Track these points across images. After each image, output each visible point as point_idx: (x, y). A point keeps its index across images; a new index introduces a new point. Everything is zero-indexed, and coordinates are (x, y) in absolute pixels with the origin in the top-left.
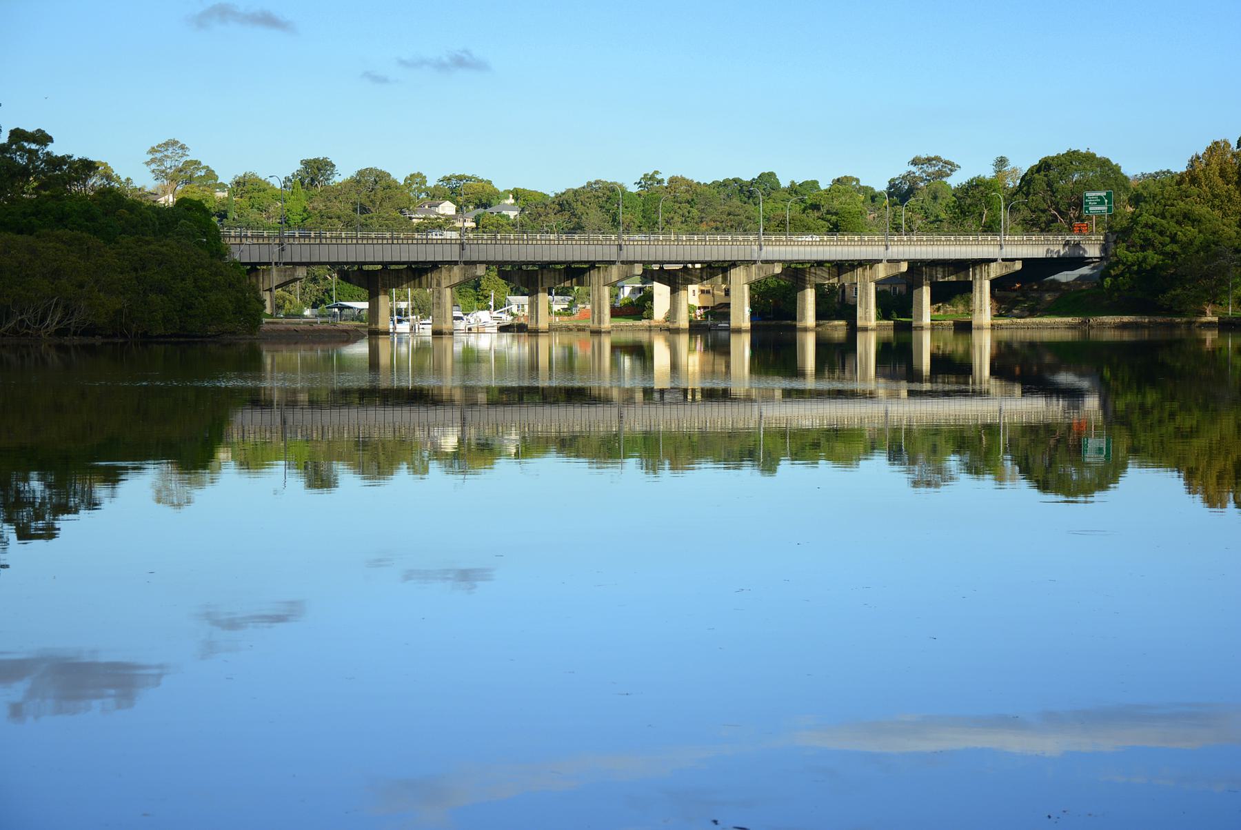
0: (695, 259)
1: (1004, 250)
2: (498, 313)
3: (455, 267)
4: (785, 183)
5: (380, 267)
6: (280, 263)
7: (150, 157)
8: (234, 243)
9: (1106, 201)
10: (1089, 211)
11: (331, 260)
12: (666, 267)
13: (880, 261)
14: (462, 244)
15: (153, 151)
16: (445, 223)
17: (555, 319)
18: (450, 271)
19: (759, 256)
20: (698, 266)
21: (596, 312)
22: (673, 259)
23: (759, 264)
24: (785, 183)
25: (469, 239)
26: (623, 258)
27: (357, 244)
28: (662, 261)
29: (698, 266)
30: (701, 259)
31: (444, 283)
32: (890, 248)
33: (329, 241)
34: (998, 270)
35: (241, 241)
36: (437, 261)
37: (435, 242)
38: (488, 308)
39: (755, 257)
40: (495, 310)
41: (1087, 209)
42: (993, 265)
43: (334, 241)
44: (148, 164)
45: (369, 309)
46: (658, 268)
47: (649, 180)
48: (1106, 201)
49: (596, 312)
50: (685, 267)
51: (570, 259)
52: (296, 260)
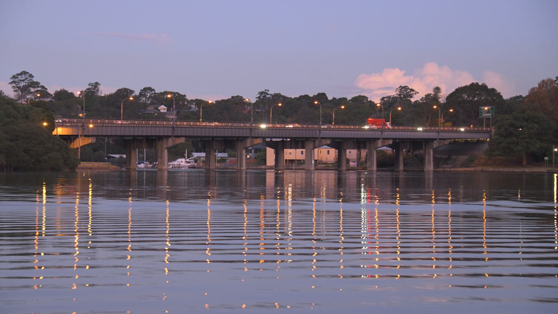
0: (287, 136)
1: (440, 134)
2: (189, 160)
3: (317, 140)
4: (330, 98)
5: (131, 138)
6: (82, 135)
7: (12, 80)
8: (59, 125)
9: (491, 111)
10: (482, 116)
11: (108, 134)
12: (274, 140)
13: (379, 139)
14: (173, 127)
15: (14, 77)
16: (161, 117)
17: (217, 165)
18: (167, 140)
19: (319, 135)
20: (288, 140)
21: (239, 161)
22: (277, 136)
23: (320, 139)
24: (330, 98)
25: (177, 125)
26: (175, 134)
27: (139, 126)
28: (271, 137)
29: (288, 140)
30: (291, 136)
31: (165, 146)
32: (384, 133)
33: (107, 125)
34: (437, 144)
35: (63, 124)
36: (148, 136)
37: (125, 125)
38: (184, 157)
39: (317, 136)
40: (187, 159)
41: (481, 115)
42: (435, 142)
43: (110, 125)
44: (11, 83)
45: (206, 157)
46: (269, 141)
47: (274, 94)
48: (491, 111)
49: (239, 161)
50: (283, 140)
51: (226, 135)
52: (179, 134)
